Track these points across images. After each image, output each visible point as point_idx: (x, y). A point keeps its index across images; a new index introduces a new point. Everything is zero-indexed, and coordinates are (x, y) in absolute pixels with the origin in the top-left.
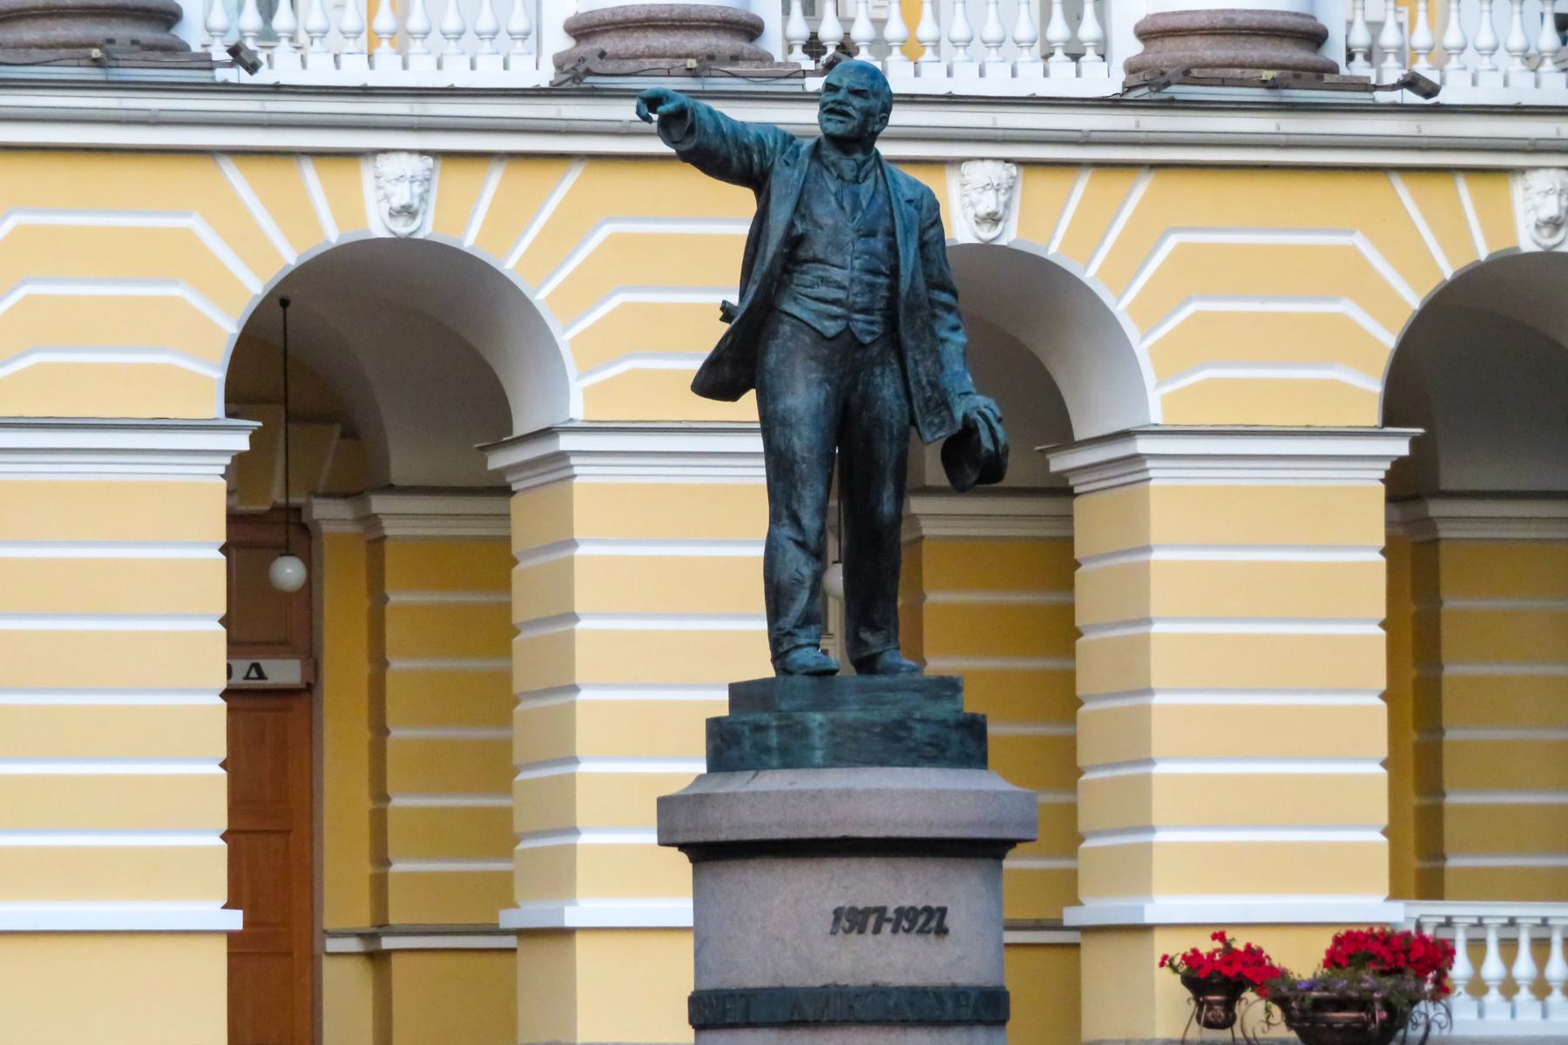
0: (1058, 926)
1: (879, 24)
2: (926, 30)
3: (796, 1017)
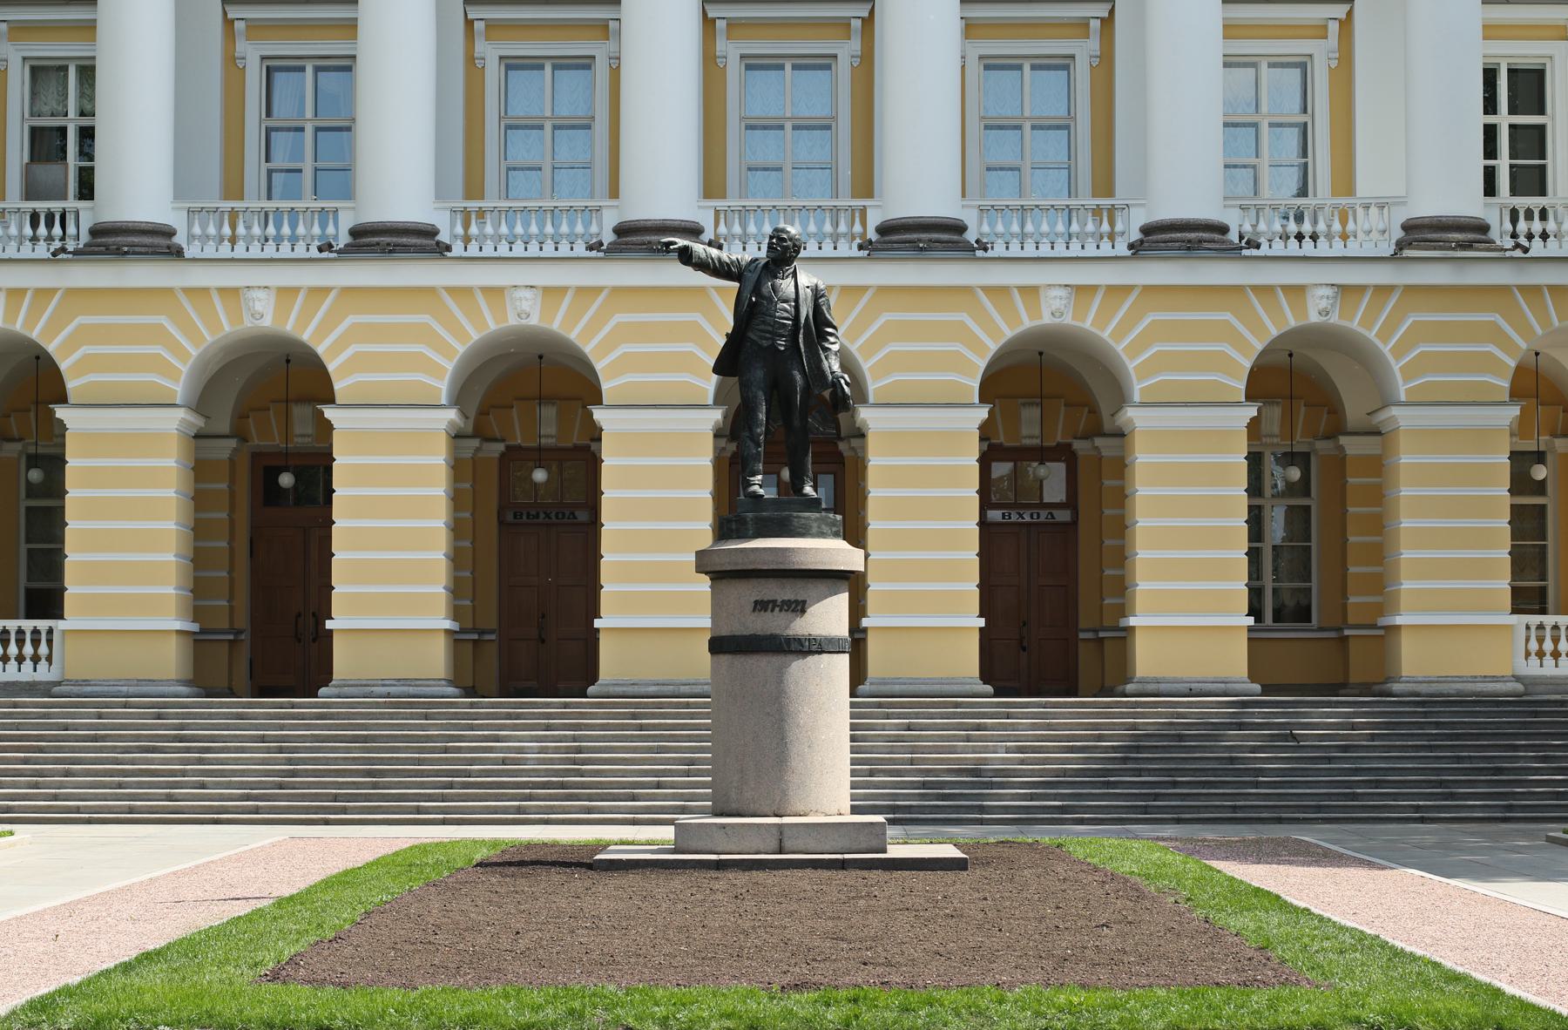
0: (1374, 627)
1: (1329, 226)
2: (1321, 227)
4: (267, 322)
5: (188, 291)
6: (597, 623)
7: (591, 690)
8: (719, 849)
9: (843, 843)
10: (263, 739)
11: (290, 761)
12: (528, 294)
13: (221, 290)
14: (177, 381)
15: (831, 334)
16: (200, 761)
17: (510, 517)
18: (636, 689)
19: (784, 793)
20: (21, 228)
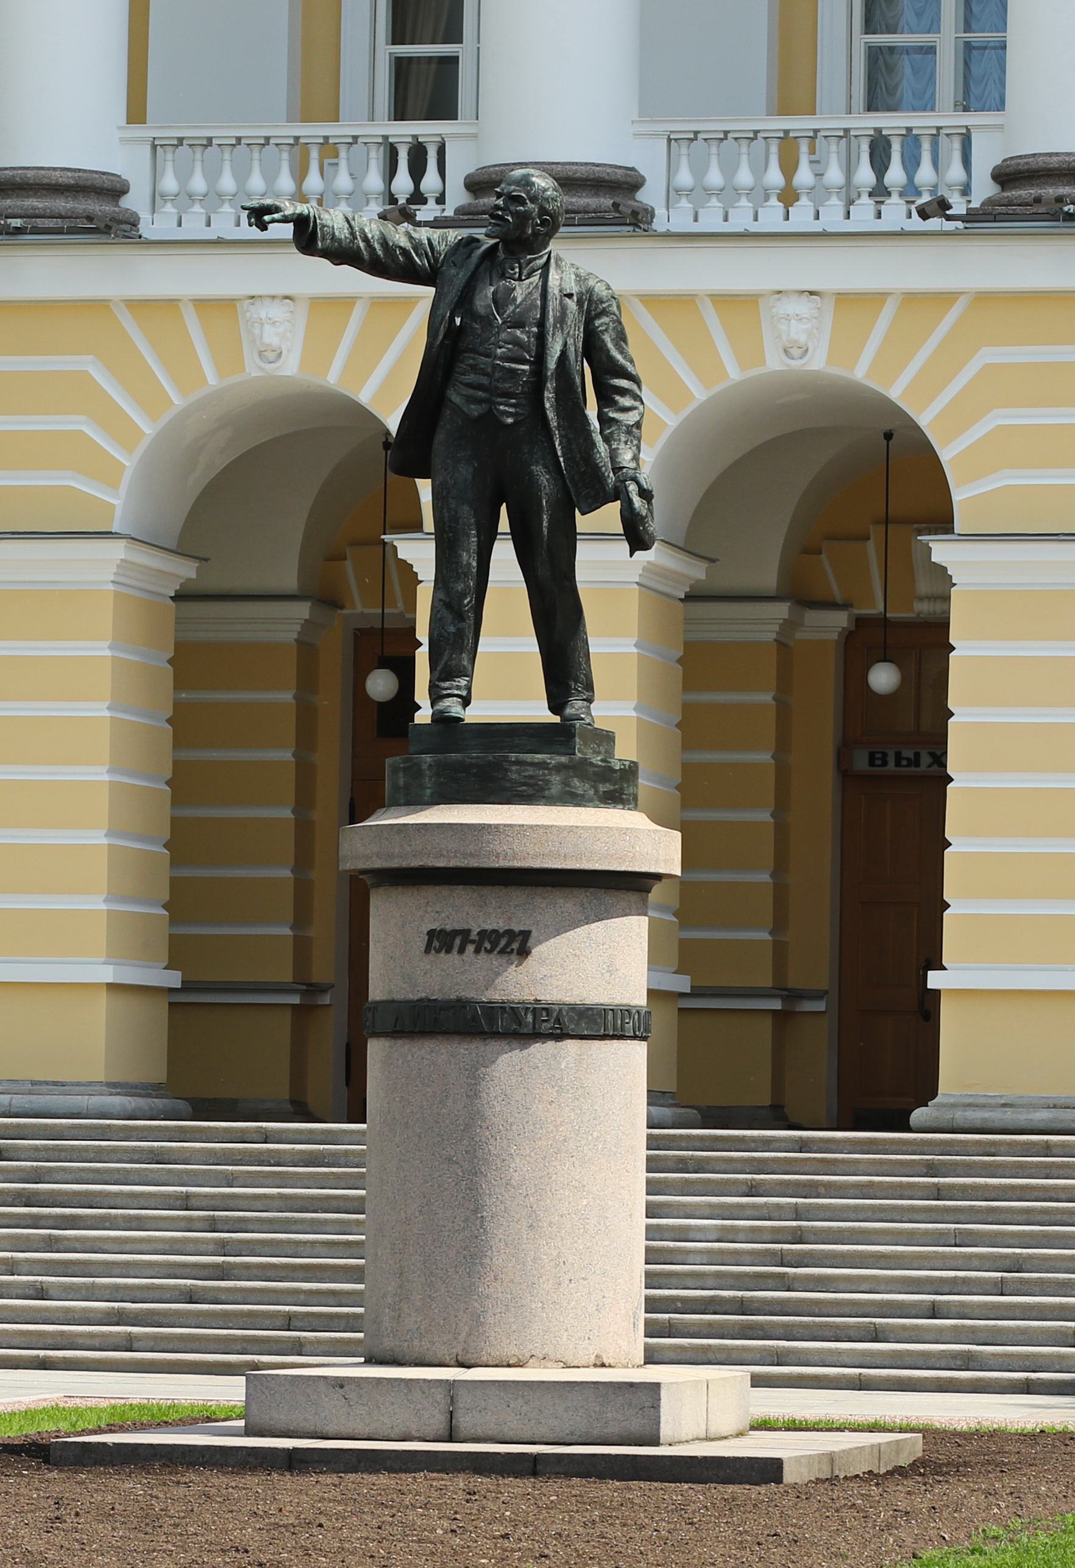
3: (398, 1028)
4: (290, 367)
5: (136, 305)
6: (935, 980)
7: (919, 1115)
8: (331, 1429)
9: (578, 1423)
10: (186, 1202)
11: (223, 1248)
12: (803, 307)
13: (201, 303)
14: (114, 485)
15: (623, 392)
16: (51, 1245)
17: (861, 762)
18: (1009, 1117)
19: (477, 1320)
20: (849, 171)
